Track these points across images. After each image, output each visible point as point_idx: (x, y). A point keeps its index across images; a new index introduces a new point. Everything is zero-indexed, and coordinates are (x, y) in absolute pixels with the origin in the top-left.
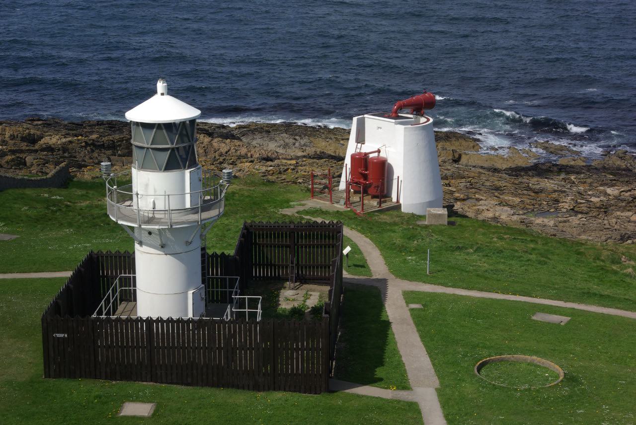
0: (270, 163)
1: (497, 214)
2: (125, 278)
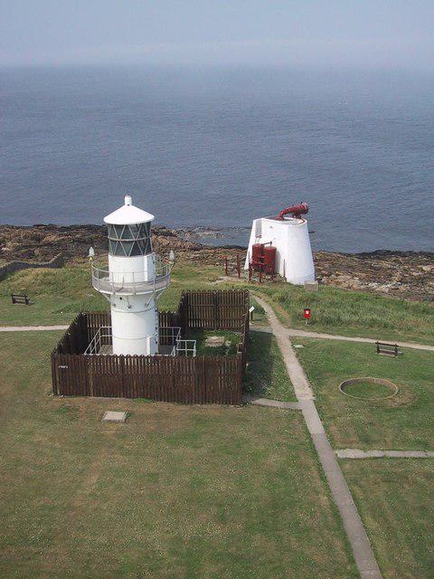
0: (197, 252)
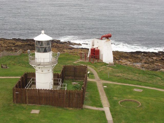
0: (71, 50)
1: (127, 63)
2: (33, 79)
